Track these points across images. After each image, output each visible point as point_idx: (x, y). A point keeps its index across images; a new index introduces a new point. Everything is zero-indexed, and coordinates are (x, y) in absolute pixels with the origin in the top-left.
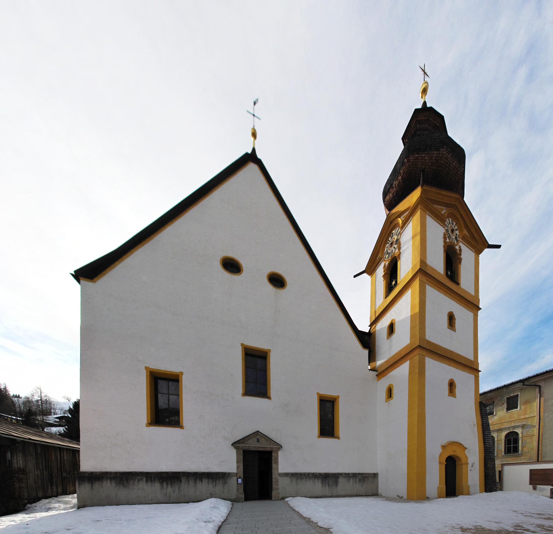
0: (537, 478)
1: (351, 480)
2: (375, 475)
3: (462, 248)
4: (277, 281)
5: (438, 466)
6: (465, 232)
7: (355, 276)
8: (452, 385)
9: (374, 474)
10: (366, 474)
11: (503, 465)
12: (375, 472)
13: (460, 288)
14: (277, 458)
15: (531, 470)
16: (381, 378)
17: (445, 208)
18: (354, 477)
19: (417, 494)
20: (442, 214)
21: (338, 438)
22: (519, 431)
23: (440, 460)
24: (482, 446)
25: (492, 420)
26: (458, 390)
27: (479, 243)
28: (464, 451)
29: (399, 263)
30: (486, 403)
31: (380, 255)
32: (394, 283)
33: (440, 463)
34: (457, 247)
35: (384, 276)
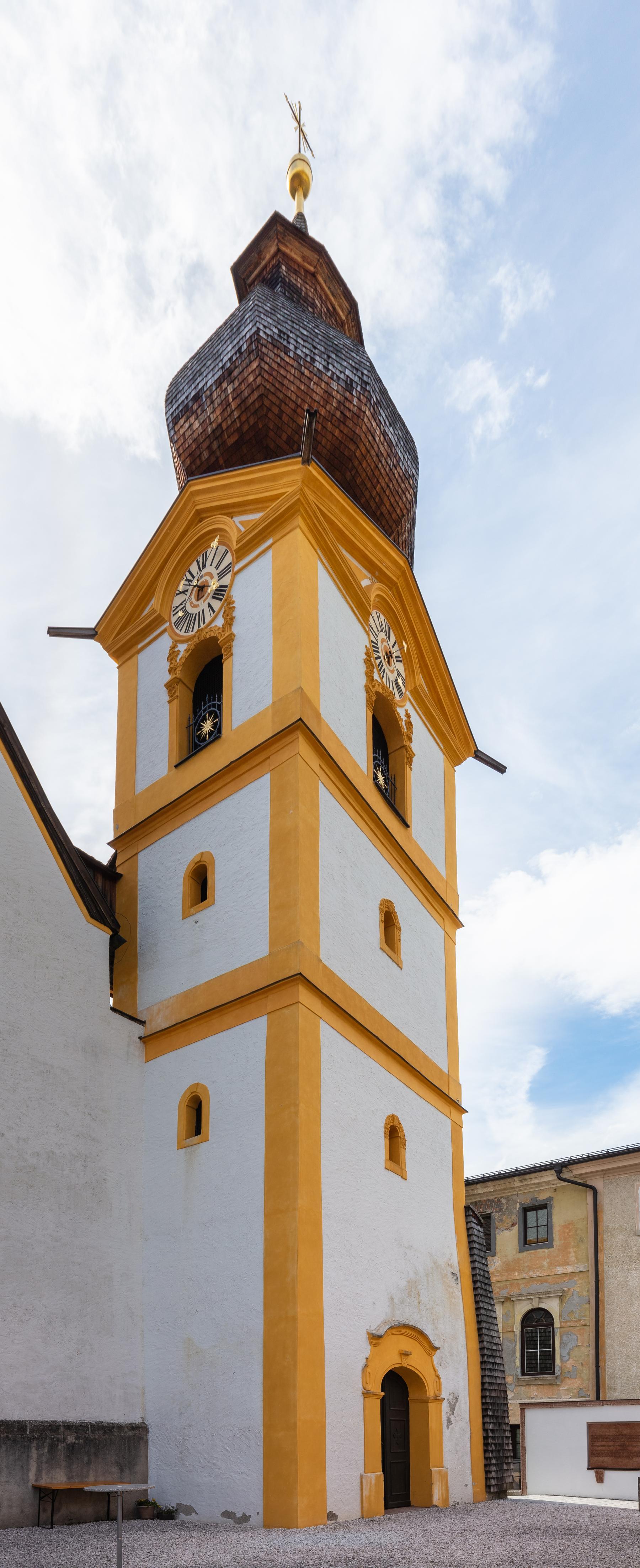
0: (612, 1449)
1: (34, 1453)
3: (411, 719)
5: (358, 1402)
6: (420, 680)
7: (54, 632)
8: (394, 1133)
9: (133, 1427)
11: (524, 1407)
13: (409, 837)
15: (592, 1427)
17: (369, 575)
20: (359, 586)
22: (553, 1306)
23: (364, 1382)
24: (475, 1345)
25: (495, 1265)
26: (411, 1153)
27: (458, 742)
28: (431, 1355)
29: (226, 665)
30: (489, 1210)
31: (154, 603)
32: (207, 726)
33: (367, 1394)
34: (401, 712)
35: (169, 686)
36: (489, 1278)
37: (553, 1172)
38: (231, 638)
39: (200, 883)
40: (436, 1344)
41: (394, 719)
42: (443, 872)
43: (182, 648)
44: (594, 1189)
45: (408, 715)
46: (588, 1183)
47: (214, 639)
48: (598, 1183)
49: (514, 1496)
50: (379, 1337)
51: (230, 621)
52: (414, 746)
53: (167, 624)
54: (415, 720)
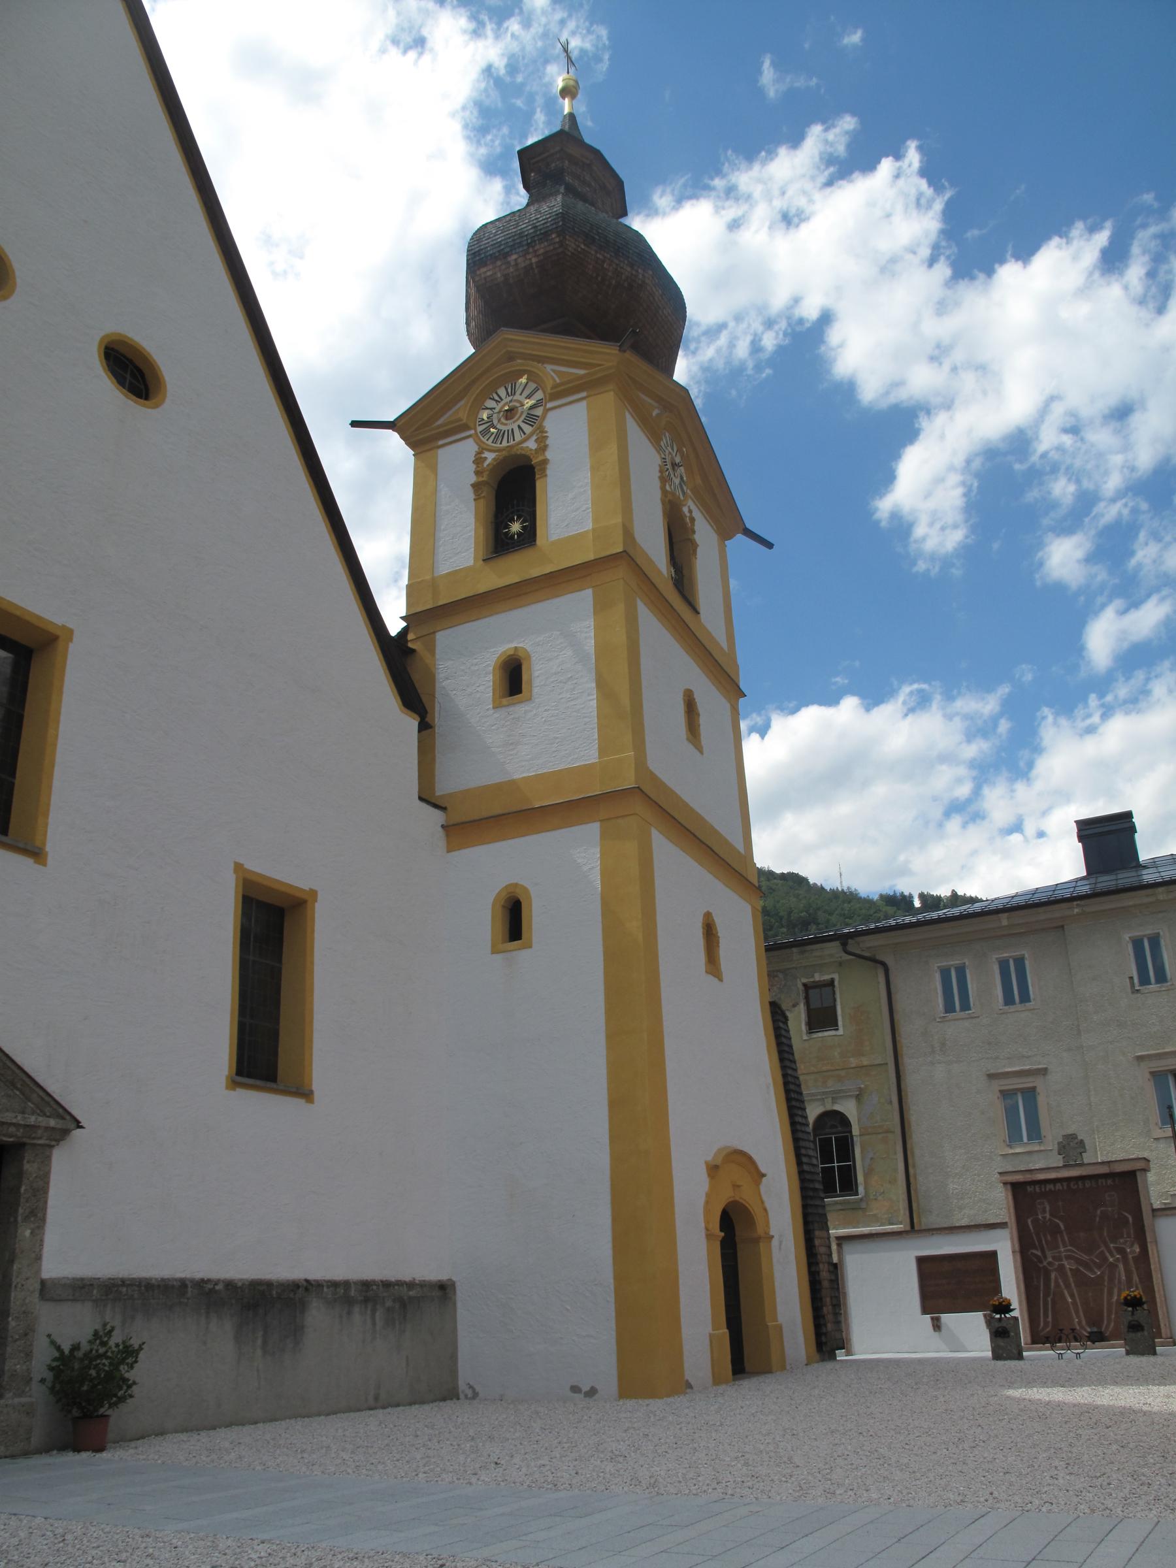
2: (444, 1290)
4: (131, 371)
10: (411, 1285)
12: (443, 1276)
14: (41, 1192)
15: (921, 1261)
16: (461, 847)
18: (366, 1300)
19: (645, 1370)
21: (306, 1094)
22: (849, 1108)
27: (729, 521)
33: (709, 1236)
34: (685, 510)
36: (799, 1086)
37: (837, 943)
38: (545, 462)
39: (513, 678)
40: (763, 1170)
41: (681, 517)
42: (725, 645)
43: (490, 457)
44: (883, 964)
45: (690, 511)
46: (878, 957)
47: (527, 458)
48: (890, 961)
49: (841, 1355)
50: (716, 1167)
51: (543, 448)
52: (697, 537)
53: (472, 432)
54: (697, 514)
